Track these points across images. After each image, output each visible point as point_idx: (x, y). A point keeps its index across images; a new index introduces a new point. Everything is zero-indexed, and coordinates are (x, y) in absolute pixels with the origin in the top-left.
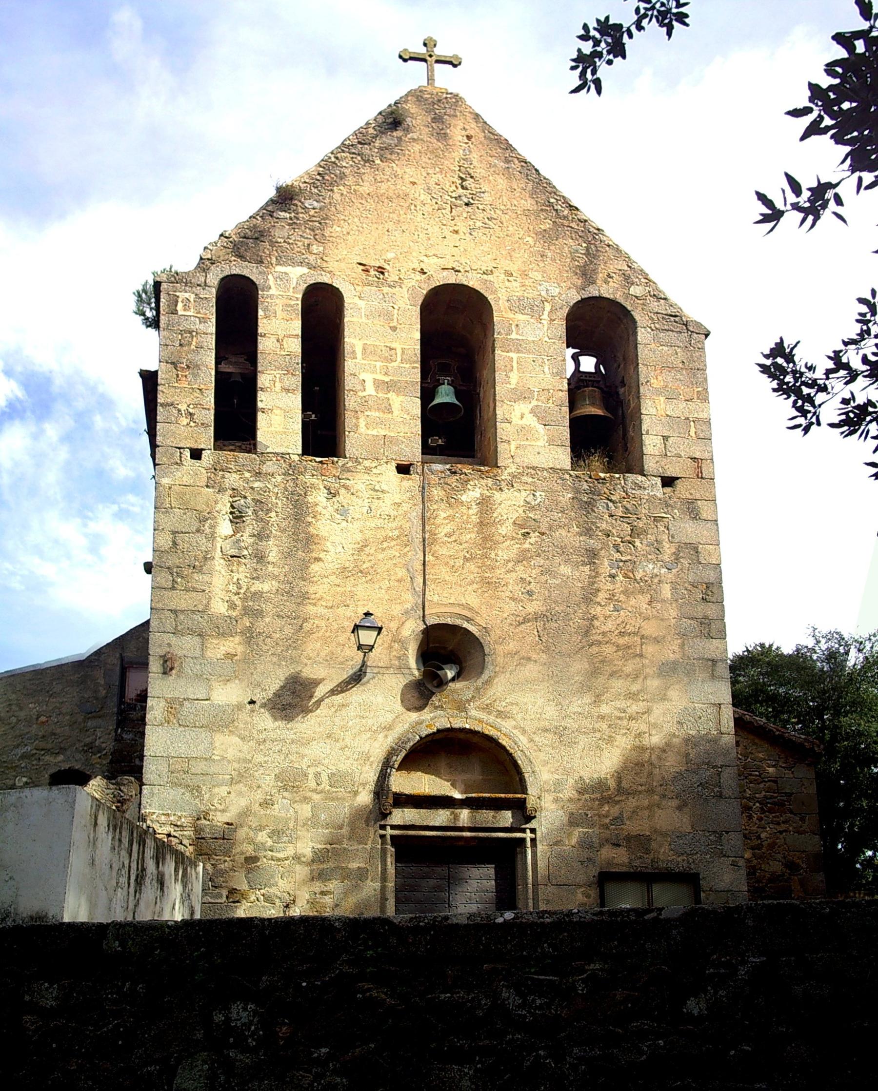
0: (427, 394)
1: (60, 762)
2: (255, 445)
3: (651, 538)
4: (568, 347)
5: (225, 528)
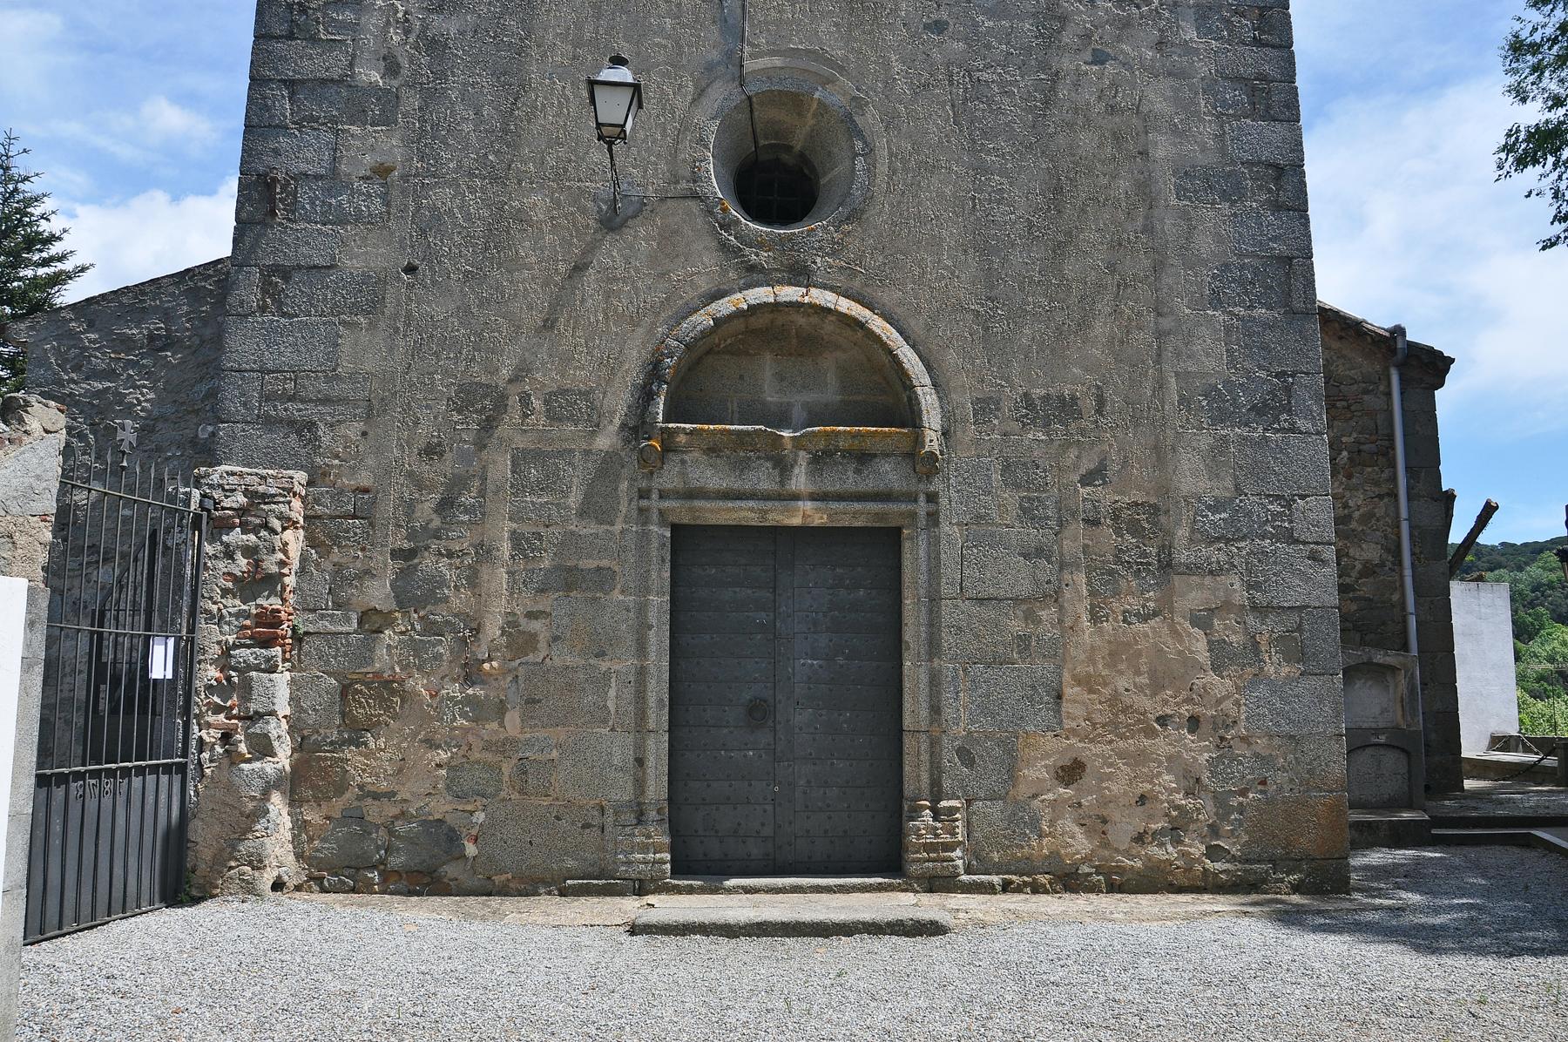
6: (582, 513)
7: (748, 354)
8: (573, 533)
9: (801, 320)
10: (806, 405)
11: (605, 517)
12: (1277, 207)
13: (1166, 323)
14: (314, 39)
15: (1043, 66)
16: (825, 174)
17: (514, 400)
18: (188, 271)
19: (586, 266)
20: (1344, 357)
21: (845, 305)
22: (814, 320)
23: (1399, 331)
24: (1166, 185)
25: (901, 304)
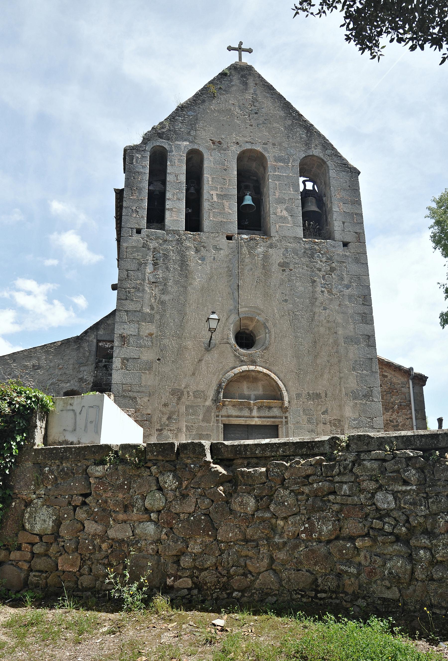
0: (240, 200)
1: (67, 387)
2: (164, 225)
3: (338, 272)
4: (300, 177)
5: (149, 269)
6: (203, 421)
7: (240, 382)
8: (200, 425)
9: (253, 374)
10: (255, 395)
11: (208, 421)
12: (369, 346)
13: (342, 375)
14: (132, 300)
15: (311, 311)
16: (258, 336)
17: (185, 393)
18: (45, 345)
19: (202, 360)
20: (396, 376)
21: (265, 371)
22: (257, 374)
23: (411, 369)
24: (341, 341)
25: (278, 370)
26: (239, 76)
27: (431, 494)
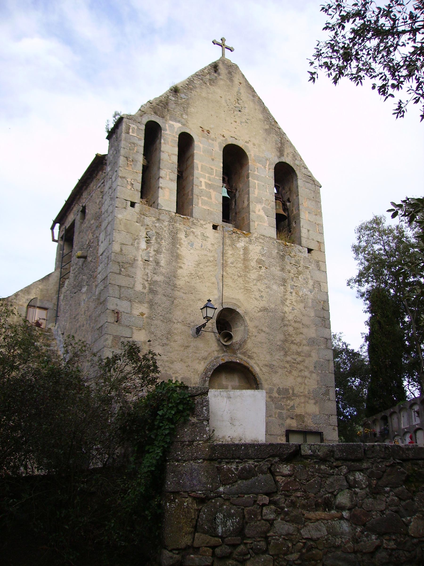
5: (143, 245)
26: (219, 71)
27: (309, 492)
